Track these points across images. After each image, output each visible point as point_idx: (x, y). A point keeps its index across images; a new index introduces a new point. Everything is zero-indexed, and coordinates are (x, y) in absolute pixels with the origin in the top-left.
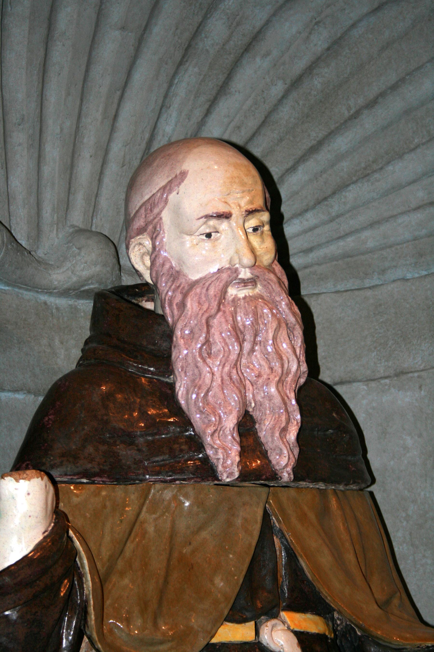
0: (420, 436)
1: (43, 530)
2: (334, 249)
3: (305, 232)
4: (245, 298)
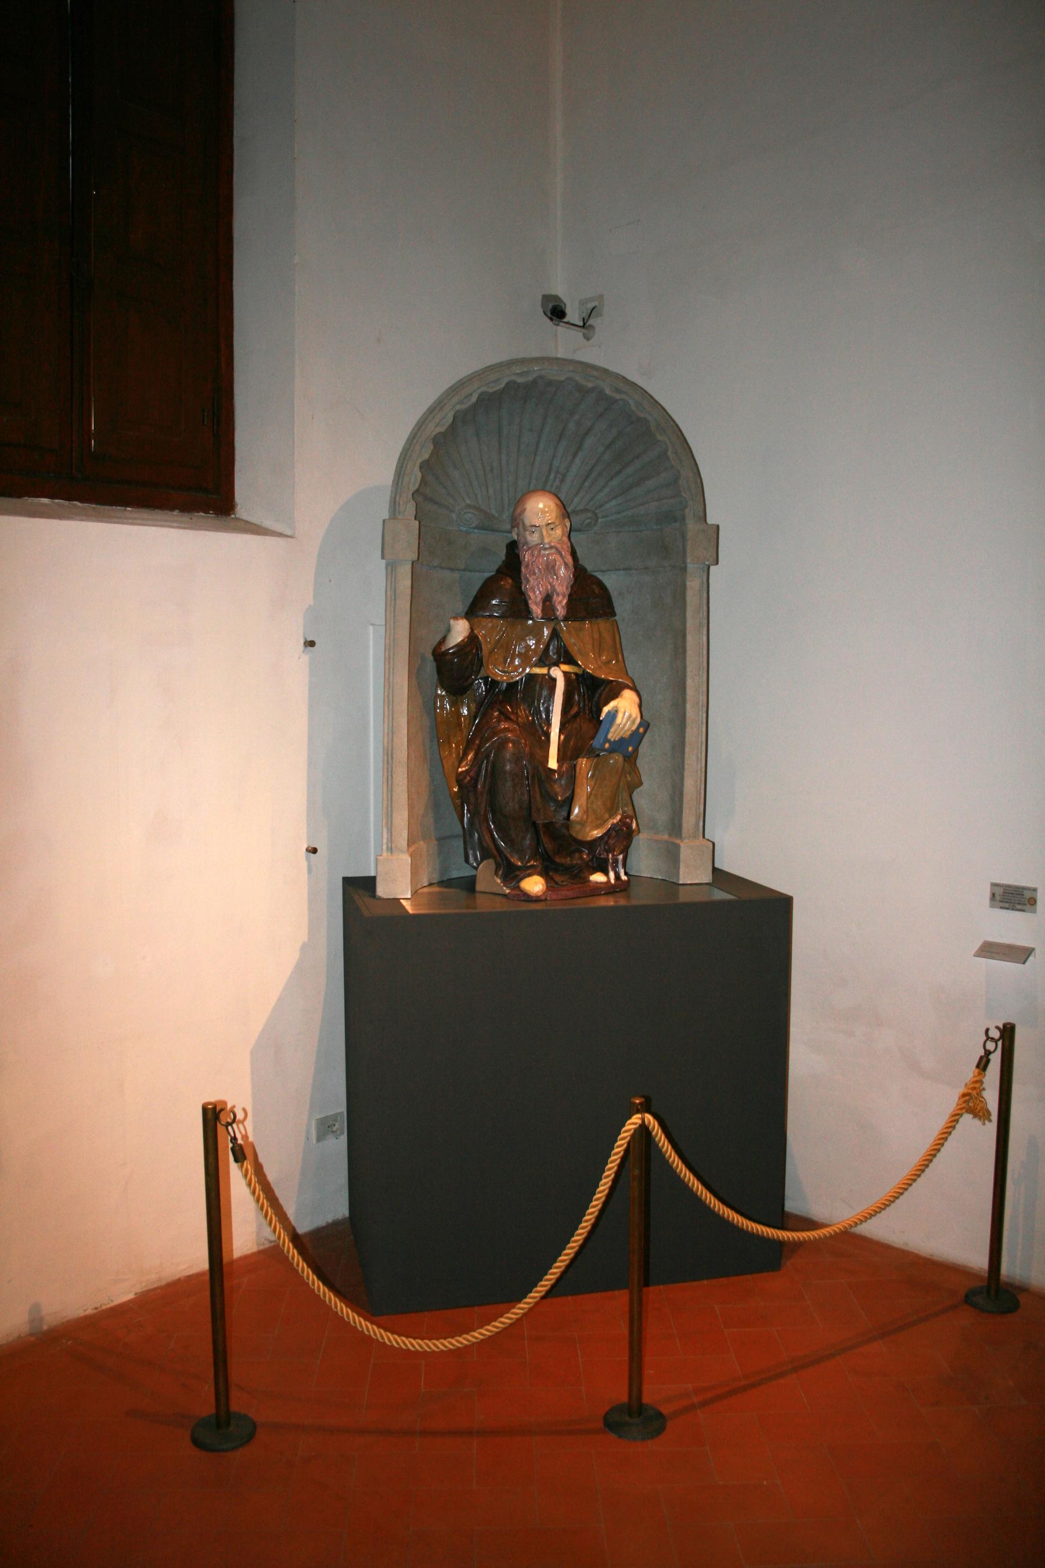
2: (629, 513)
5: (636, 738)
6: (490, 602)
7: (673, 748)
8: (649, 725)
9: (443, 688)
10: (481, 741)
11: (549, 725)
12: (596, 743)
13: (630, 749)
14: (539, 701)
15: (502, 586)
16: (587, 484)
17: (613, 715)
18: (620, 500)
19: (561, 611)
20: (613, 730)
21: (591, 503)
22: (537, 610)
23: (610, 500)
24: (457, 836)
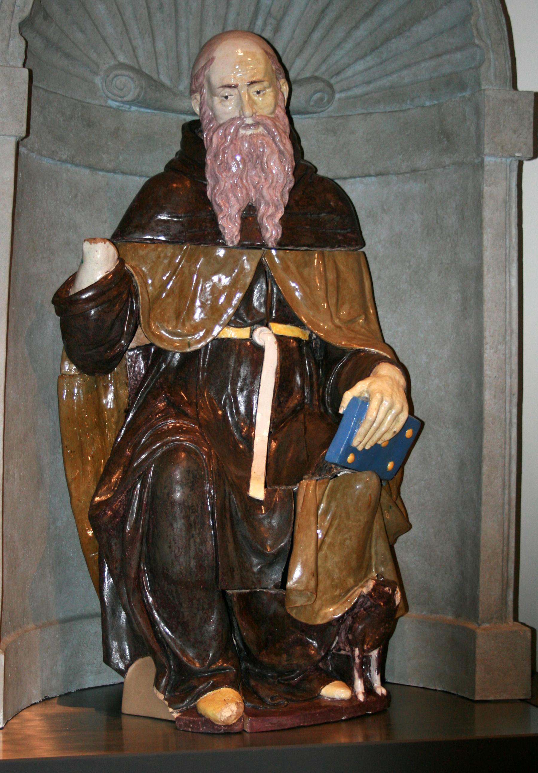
0: (422, 213)
1: (106, 271)
2: (385, 82)
3: (366, 70)
4: (250, 135)
5: (401, 446)
6: (153, 217)
7: (462, 466)
8: (422, 424)
9: (73, 361)
10: (133, 453)
11: (252, 425)
12: (332, 454)
13: (390, 465)
14: (234, 384)
15: (177, 198)
16: (316, 36)
17: (361, 405)
18: (370, 61)
19: (272, 231)
20: (361, 431)
21: (323, 68)
22: (231, 228)
23: (354, 62)
24: (91, 616)
